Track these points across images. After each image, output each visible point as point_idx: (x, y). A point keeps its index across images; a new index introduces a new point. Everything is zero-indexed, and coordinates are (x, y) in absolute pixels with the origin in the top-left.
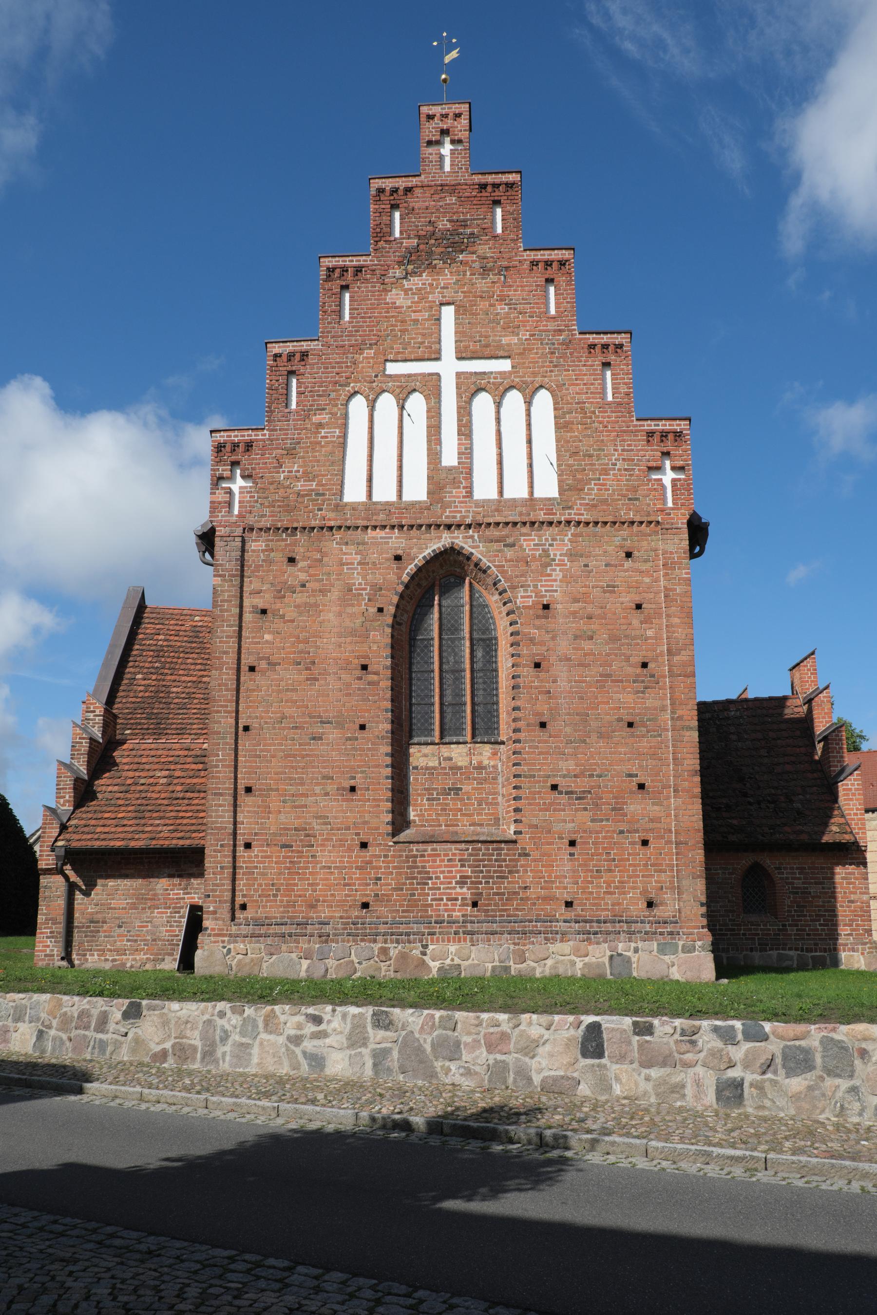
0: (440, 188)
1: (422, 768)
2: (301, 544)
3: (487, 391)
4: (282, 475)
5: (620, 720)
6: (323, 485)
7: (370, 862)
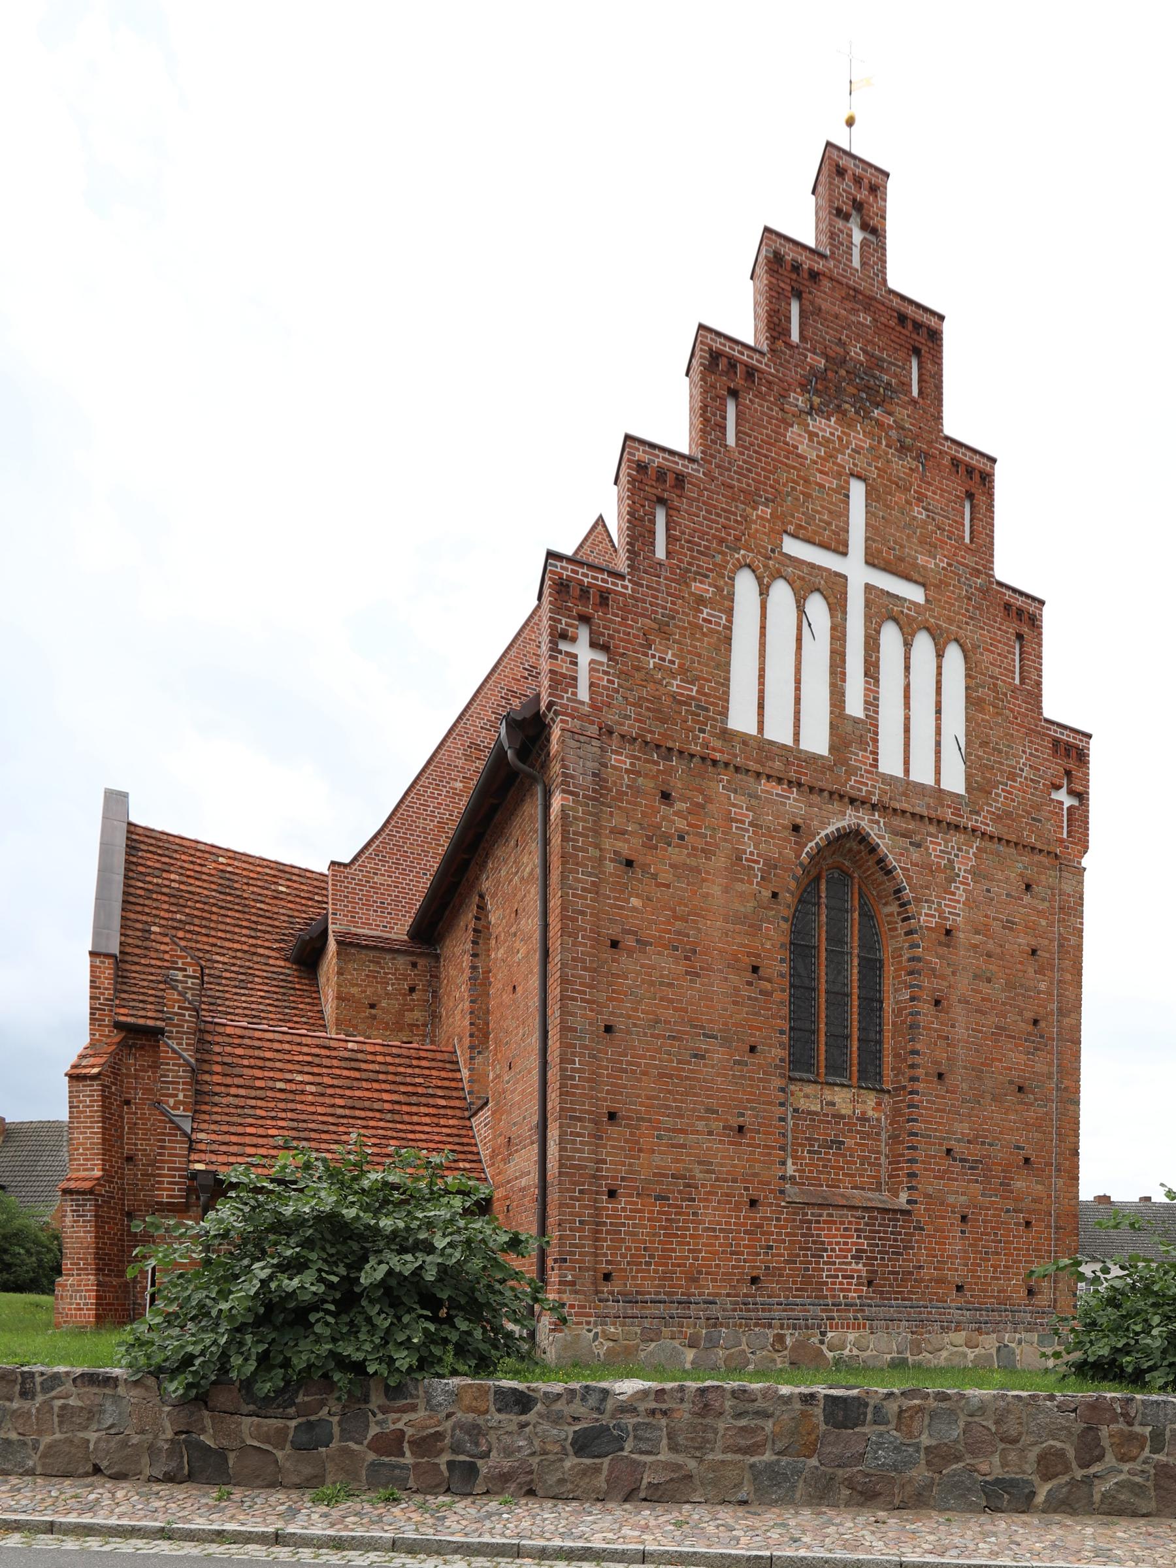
0: (852, 292)
1: (803, 1112)
2: (679, 775)
3: (898, 624)
4: (651, 661)
5: (1011, 1082)
6: (705, 694)
7: (760, 1226)
